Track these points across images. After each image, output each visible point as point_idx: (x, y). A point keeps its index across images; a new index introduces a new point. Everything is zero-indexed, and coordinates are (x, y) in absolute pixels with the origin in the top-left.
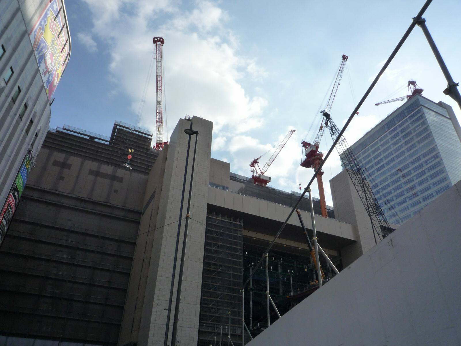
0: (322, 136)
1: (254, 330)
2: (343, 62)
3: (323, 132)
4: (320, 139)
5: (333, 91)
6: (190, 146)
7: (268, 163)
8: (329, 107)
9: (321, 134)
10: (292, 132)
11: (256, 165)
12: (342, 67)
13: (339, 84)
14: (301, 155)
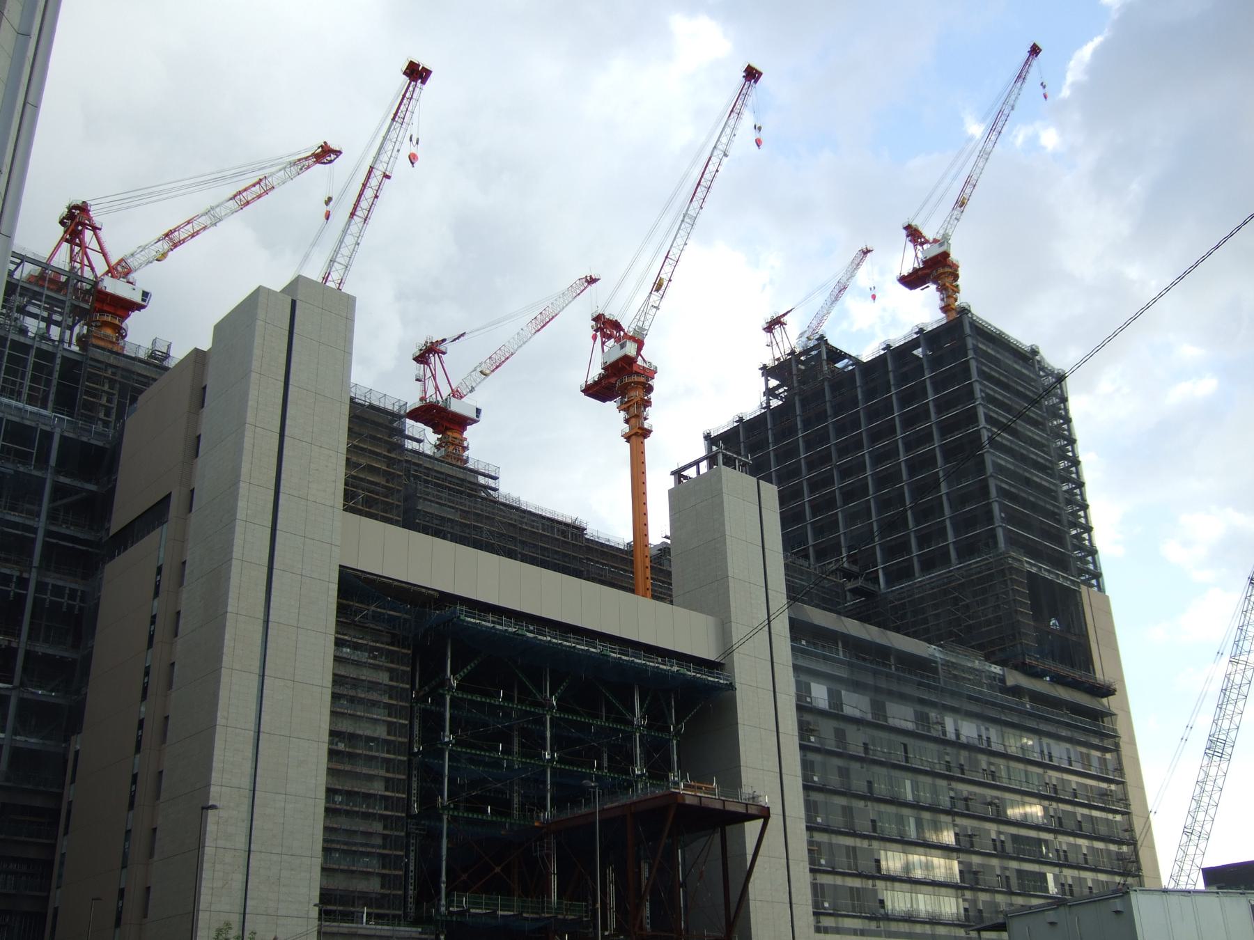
0: (657, 308)
1: (451, 913)
6: (291, 382)
11: (433, 359)
13: (726, 155)
14: (591, 360)
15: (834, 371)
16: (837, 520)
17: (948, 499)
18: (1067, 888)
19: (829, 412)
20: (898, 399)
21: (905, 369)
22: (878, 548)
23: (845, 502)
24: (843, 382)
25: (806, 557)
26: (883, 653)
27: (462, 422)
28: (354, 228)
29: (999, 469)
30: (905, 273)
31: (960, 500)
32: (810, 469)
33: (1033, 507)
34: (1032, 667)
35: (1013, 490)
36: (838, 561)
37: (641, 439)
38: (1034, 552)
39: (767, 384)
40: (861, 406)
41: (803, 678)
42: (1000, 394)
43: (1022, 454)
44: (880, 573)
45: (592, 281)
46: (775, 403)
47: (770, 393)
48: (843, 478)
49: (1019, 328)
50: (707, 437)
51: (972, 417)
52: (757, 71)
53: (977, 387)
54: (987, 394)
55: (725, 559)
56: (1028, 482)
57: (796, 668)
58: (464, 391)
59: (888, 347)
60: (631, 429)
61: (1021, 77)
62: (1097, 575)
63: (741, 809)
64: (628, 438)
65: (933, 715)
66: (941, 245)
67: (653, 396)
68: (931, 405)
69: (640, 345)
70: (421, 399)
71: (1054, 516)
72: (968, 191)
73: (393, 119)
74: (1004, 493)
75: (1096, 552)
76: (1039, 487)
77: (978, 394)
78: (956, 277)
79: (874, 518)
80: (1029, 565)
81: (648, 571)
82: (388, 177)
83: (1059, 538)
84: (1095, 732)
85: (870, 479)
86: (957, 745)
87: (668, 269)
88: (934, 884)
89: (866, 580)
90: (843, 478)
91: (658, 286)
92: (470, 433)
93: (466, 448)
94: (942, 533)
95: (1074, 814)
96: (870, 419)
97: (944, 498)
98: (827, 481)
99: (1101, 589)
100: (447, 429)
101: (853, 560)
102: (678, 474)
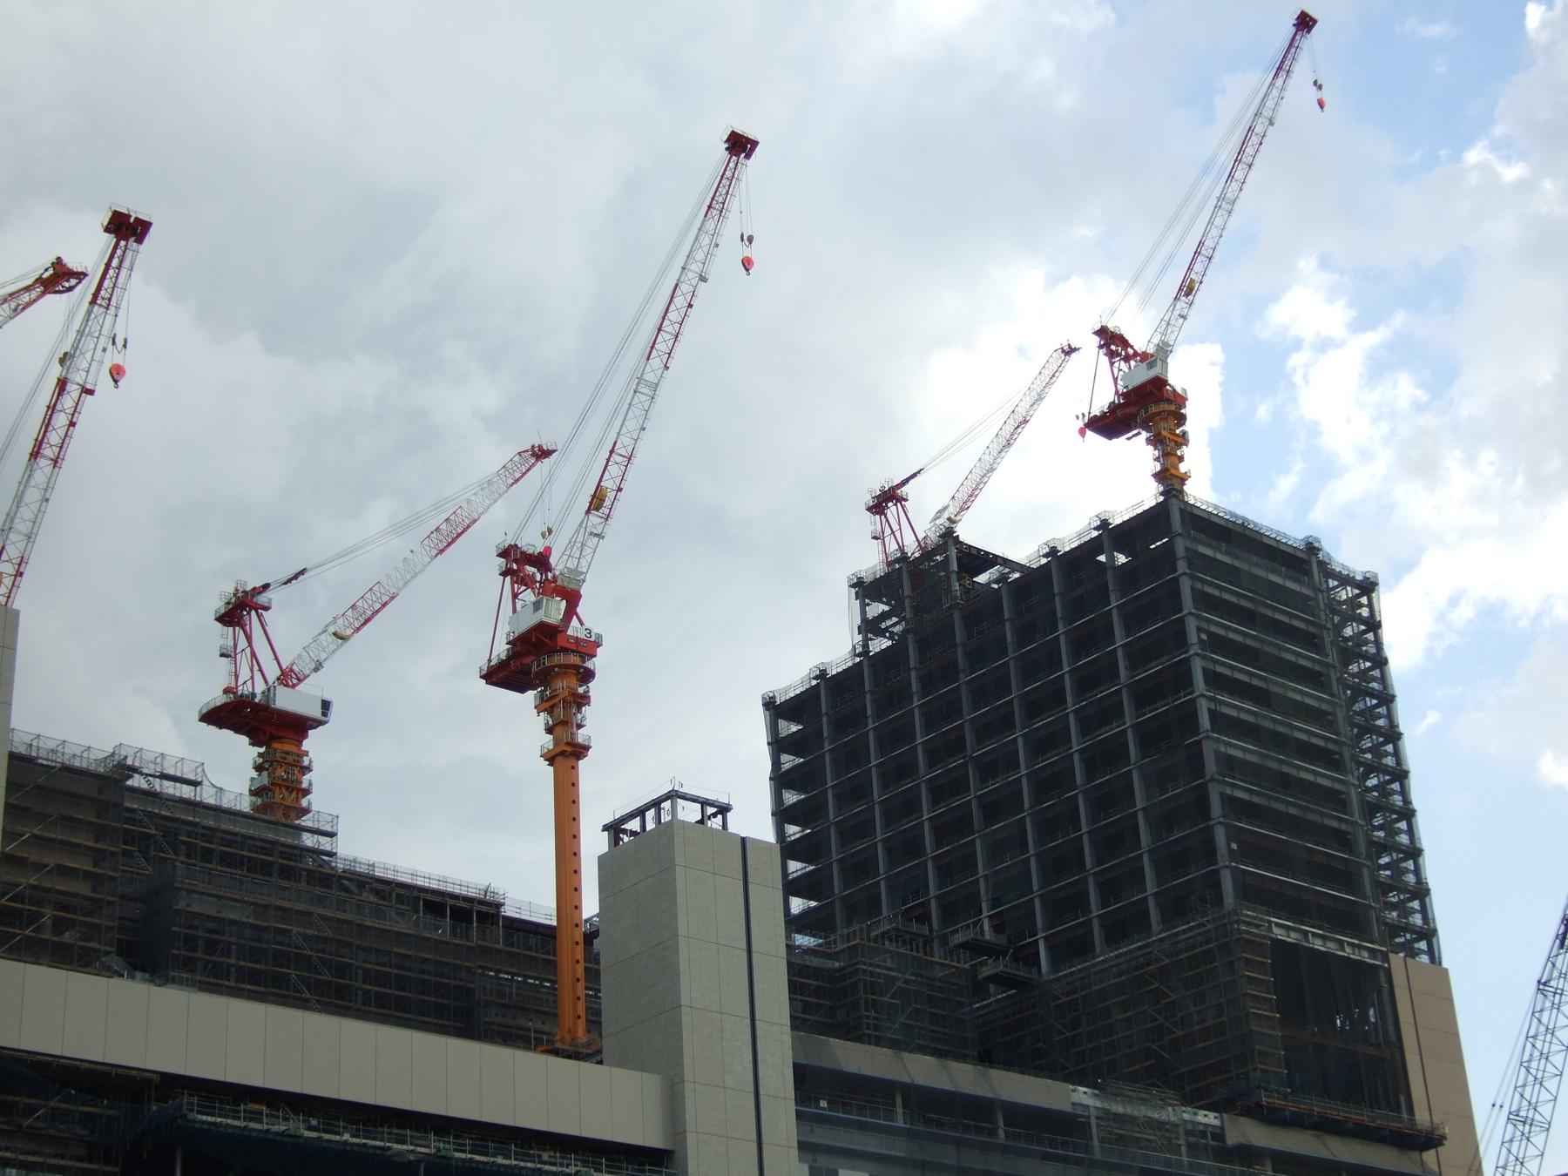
2: (732, 165)
4: (587, 551)
7: (340, 621)
11: (892, 510)
13: (703, 279)
17: (1147, 818)
19: (962, 662)
22: (1037, 902)
24: (984, 606)
26: (978, 1110)
27: (299, 726)
28: (40, 477)
29: (1230, 765)
30: (1096, 411)
31: (1165, 820)
32: (932, 764)
33: (1296, 825)
34: (1272, 1109)
35: (1256, 799)
36: (975, 924)
37: (572, 761)
38: (1295, 907)
39: (863, 612)
40: (1011, 655)
42: (1237, 632)
43: (1276, 734)
44: (1042, 944)
45: (541, 454)
46: (879, 644)
47: (869, 627)
48: (983, 780)
49: (1275, 510)
50: (769, 704)
51: (1182, 677)
52: (748, 140)
53: (1192, 625)
54: (1211, 635)
55: (675, 977)
56: (1286, 783)
58: (303, 667)
59: (1053, 552)
60: (556, 743)
62: (1429, 933)
64: (551, 759)
66: (1151, 366)
67: (594, 688)
68: (1120, 654)
70: (227, 691)
71: (1343, 840)
73: (93, 302)
75: (1427, 892)
77: (1193, 637)
80: (1282, 930)
81: (581, 985)
82: (91, 392)
83: (1346, 877)
85: (1024, 782)
87: (614, 470)
89: (1016, 959)
90: (983, 780)
91: (597, 501)
92: (313, 744)
93: (308, 769)
94: (1137, 877)
96: (1027, 677)
97: (1140, 816)
99: (1434, 958)
100: (274, 738)
101: (999, 925)
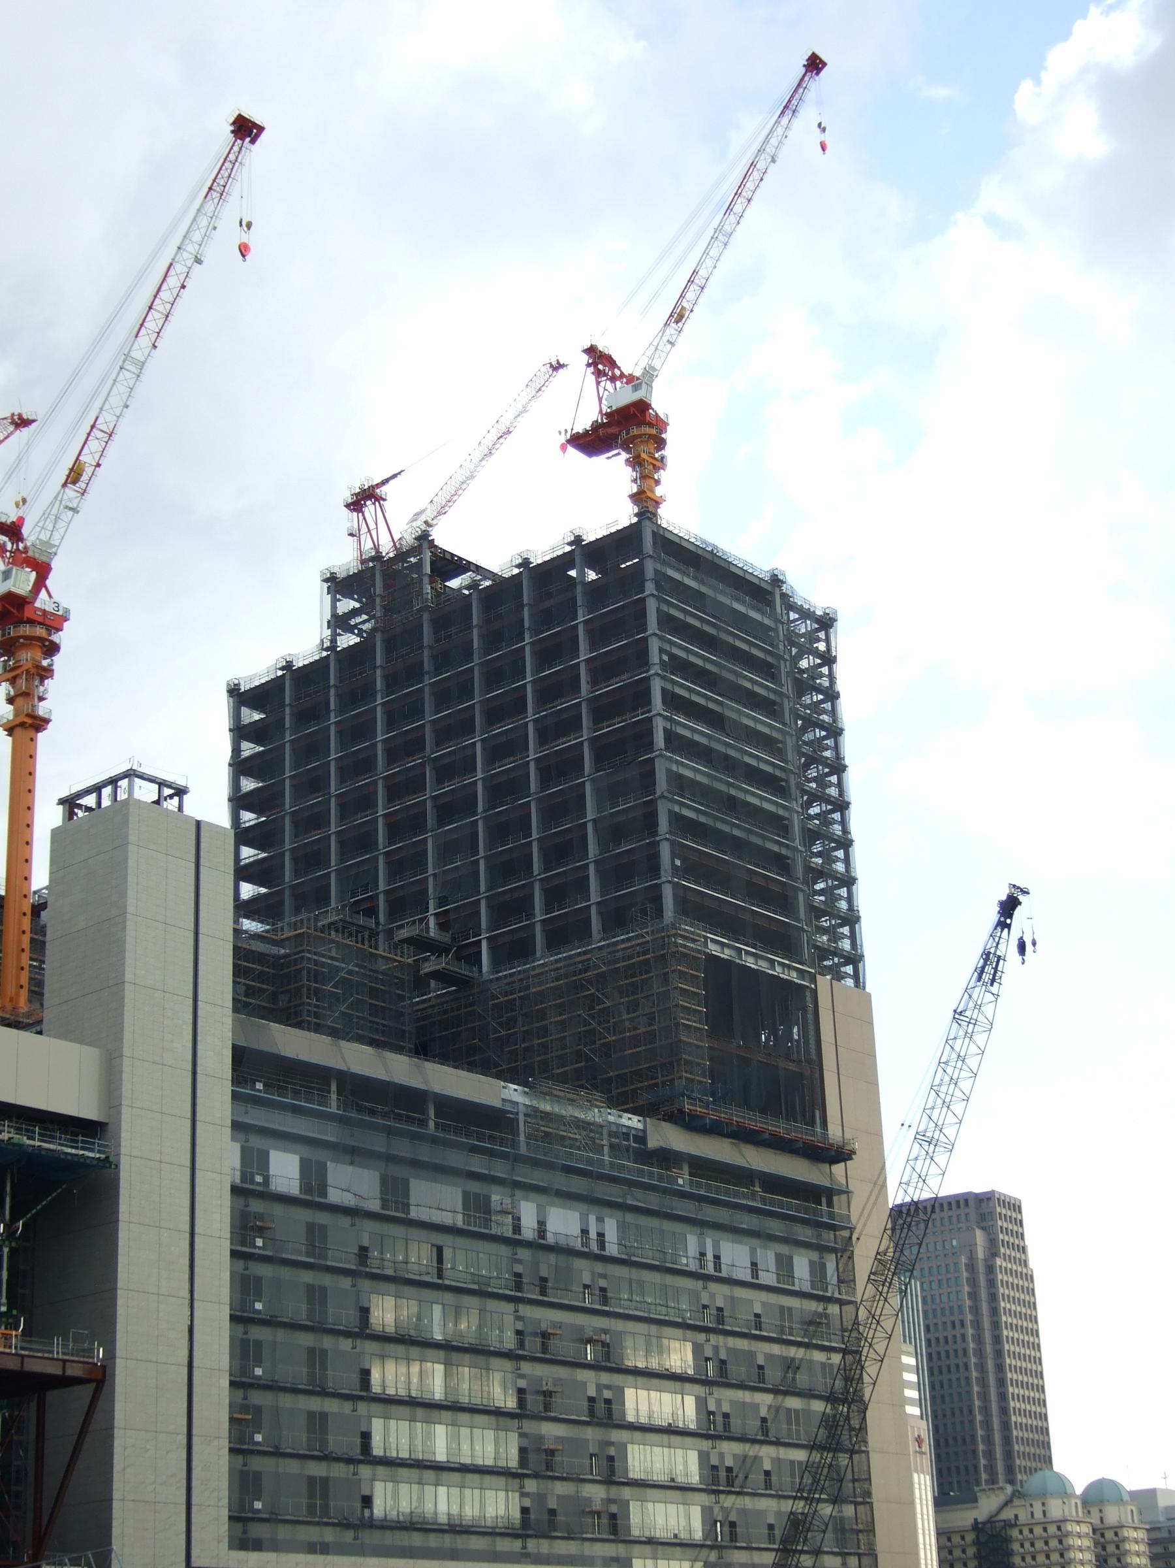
2: (236, 148)
3: (83, 494)
5: (163, 288)
8: (132, 368)
9: (70, 500)
10: (13, 422)
11: (370, 508)
12: (224, 173)
13: (198, 261)
15: (443, 595)
16: (425, 853)
17: (596, 829)
18: (723, 1474)
19: (427, 665)
20: (533, 653)
21: (548, 604)
22: (483, 904)
23: (442, 820)
24: (451, 613)
25: (372, 912)
29: (680, 784)
30: (579, 429)
33: (738, 846)
34: (694, 1117)
35: (702, 819)
36: (421, 921)
37: (31, 733)
38: (730, 925)
39: (334, 607)
41: (256, 1142)
42: (698, 656)
43: (727, 757)
44: (484, 944)
45: (21, 422)
46: (347, 640)
47: (339, 623)
51: (641, 695)
52: (255, 125)
53: (654, 645)
54: (673, 657)
56: (732, 805)
57: (237, 1127)
60: (16, 714)
61: (789, 108)
62: (855, 959)
63: (54, 1369)
65: (497, 1197)
66: (636, 388)
67: (58, 661)
69: (43, 570)
71: (782, 863)
72: (690, 296)
74: (682, 825)
75: (858, 919)
76: (755, 814)
77: (654, 657)
78: (661, 443)
79: (482, 853)
80: (717, 947)
83: (783, 900)
84: (805, 1222)
86: (540, 1245)
87: (94, 445)
88: (464, 1469)
91: (74, 475)
94: (582, 885)
95: (752, 1355)
97: (590, 827)
98: (415, 784)
102: (70, 804)
